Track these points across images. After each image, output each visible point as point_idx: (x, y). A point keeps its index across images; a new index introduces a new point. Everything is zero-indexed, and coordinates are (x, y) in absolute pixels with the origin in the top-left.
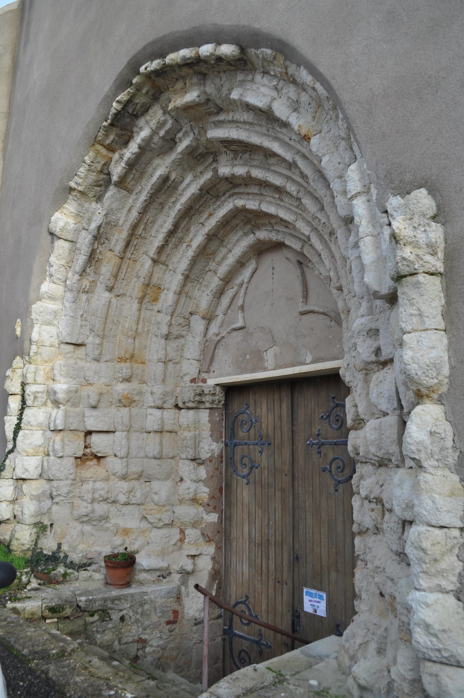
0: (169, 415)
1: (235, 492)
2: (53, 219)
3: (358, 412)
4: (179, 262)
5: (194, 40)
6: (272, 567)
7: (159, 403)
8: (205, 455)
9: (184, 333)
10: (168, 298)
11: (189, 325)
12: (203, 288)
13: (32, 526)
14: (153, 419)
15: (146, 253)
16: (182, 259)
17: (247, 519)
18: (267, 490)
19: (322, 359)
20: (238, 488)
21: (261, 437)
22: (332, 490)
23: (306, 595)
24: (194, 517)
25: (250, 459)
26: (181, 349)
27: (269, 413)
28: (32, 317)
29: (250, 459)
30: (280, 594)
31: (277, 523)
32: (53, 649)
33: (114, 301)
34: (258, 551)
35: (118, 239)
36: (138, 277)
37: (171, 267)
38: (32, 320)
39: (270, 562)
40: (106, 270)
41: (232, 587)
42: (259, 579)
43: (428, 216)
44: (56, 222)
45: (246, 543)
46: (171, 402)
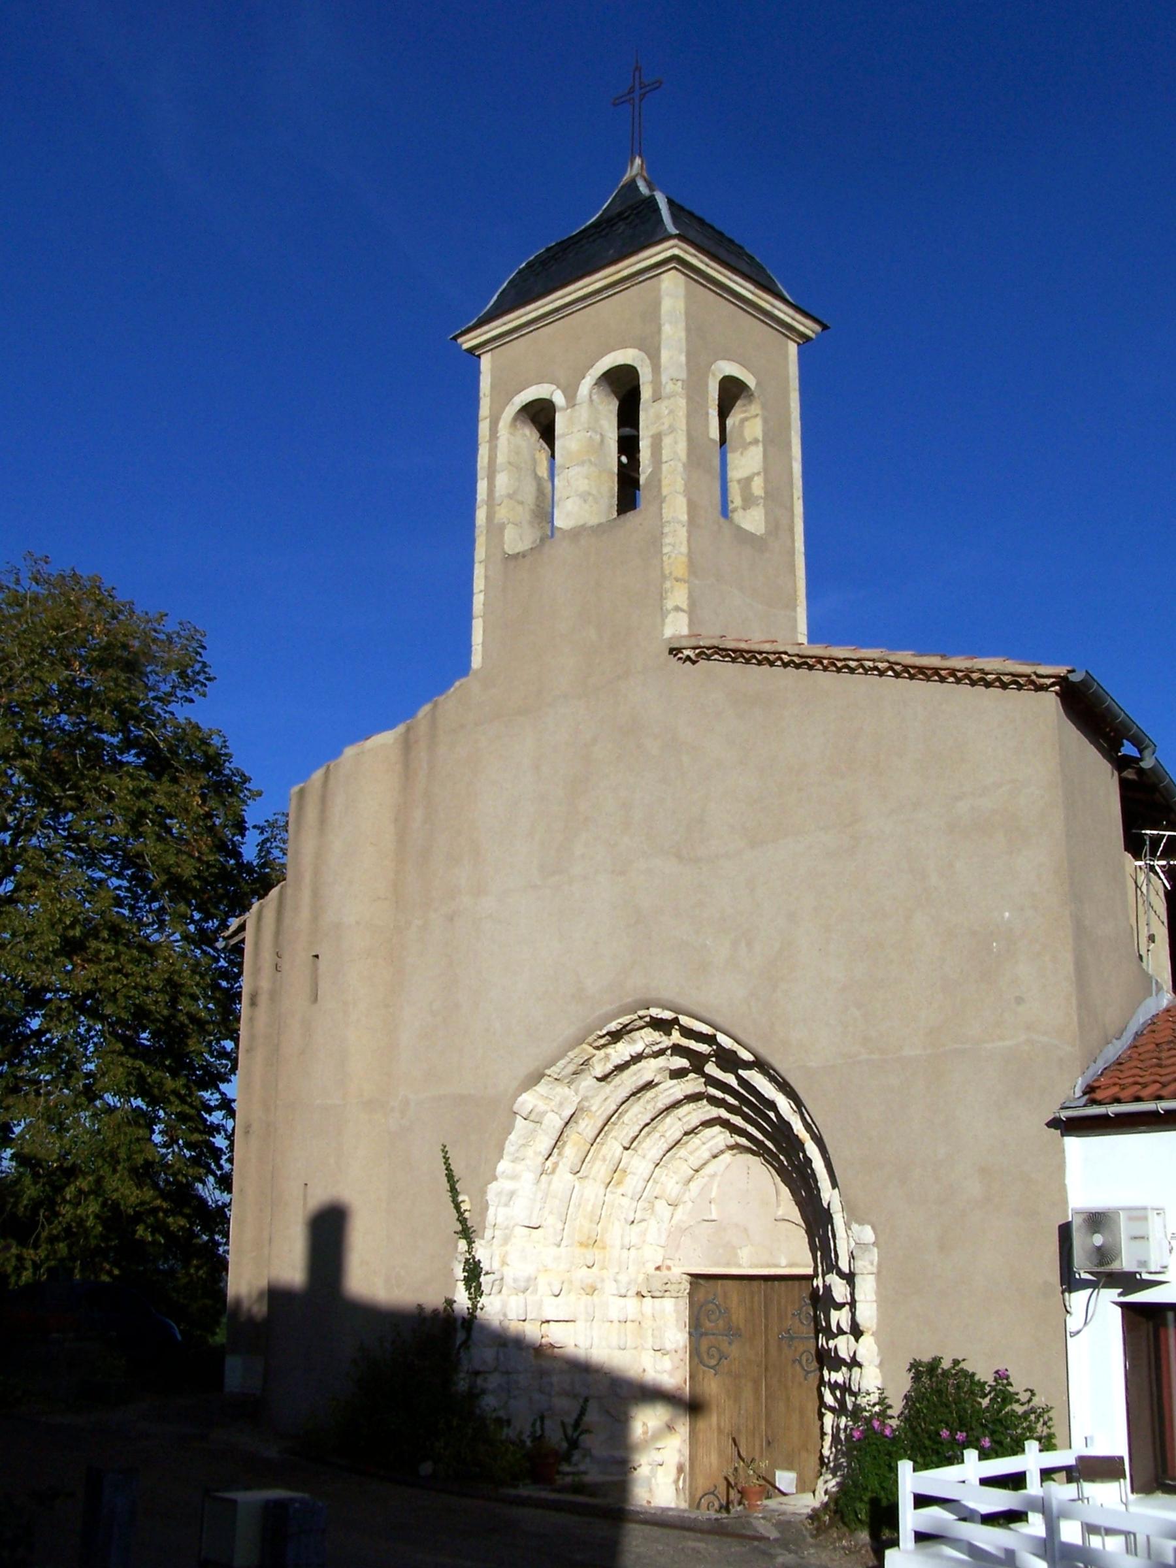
0: (632, 1303)
2: (520, 1099)
4: (649, 1149)
5: (785, 1087)
7: (623, 1292)
8: (669, 1346)
9: (647, 1217)
10: (632, 1183)
11: (653, 1208)
12: (671, 1174)
13: (555, 1437)
14: (617, 1308)
15: (616, 1138)
16: (653, 1146)
21: (730, 1328)
22: (802, 1379)
23: (1121, 1459)
25: (718, 1350)
26: (644, 1233)
29: (718, 1350)
33: (577, 1184)
35: (587, 1127)
36: (604, 1160)
37: (640, 1152)
40: (571, 1152)
44: (523, 1103)
46: (632, 1292)
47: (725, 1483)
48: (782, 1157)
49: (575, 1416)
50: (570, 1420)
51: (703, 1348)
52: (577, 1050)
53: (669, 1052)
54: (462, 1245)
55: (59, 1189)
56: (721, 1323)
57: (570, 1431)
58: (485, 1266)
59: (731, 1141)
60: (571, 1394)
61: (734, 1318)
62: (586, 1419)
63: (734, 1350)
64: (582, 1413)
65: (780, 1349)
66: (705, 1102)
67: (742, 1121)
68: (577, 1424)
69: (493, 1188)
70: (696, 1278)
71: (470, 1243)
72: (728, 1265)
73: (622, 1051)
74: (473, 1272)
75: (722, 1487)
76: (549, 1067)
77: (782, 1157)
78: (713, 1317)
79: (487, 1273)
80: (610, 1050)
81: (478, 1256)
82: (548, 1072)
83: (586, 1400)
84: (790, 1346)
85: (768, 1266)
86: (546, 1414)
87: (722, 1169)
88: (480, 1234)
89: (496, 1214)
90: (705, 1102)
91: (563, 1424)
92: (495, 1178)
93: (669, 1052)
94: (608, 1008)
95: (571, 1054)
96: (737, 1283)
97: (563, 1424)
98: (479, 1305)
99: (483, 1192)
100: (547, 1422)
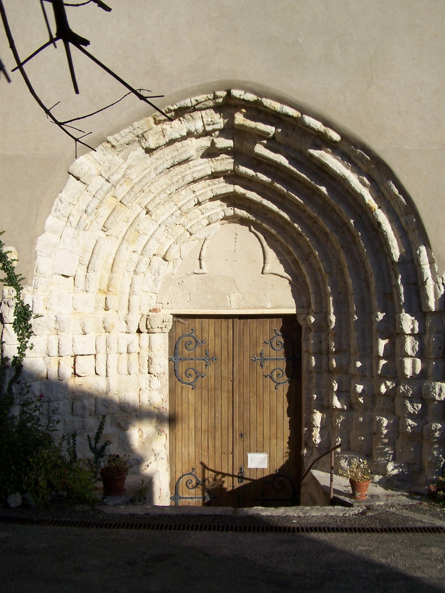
1: (180, 396)
3: (351, 402)
6: (218, 444)
17: (193, 415)
18: (213, 393)
19: (280, 307)
20: (183, 393)
24: (123, 468)
27: (216, 338)
28: (36, 249)
30: (226, 461)
31: (223, 414)
32: (301, 39)
34: (205, 436)
38: (36, 251)
39: (217, 441)
41: (177, 464)
42: (206, 454)
43: (111, 177)
45: (191, 432)
47: (200, 466)
48: (296, 225)
49: (96, 431)
50: (93, 435)
51: (181, 369)
52: (142, 122)
53: (217, 133)
54: (9, 292)
55: (315, 136)
56: (198, 350)
57: (93, 442)
58: (37, 309)
59: (230, 212)
60: (95, 414)
61: (211, 347)
62: (104, 432)
63: (211, 371)
64: (101, 428)
65: (251, 367)
66: (222, 179)
67: (258, 196)
68: (97, 438)
69: (42, 240)
70: (176, 316)
71: (19, 289)
72: (217, 307)
73: (178, 128)
74: (24, 315)
75: (199, 470)
76: (111, 134)
77: (296, 225)
78: (191, 346)
79: (37, 316)
80: (166, 126)
81: (27, 301)
82: (110, 138)
83: (104, 417)
84: (262, 366)
85: (256, 308)
86: (78, 432)
87: (213, 234)
88: (29, 282)
89: (44, 263)
90: (222, 179)
91: (89, 438)
92: (43, 231)
93: (217, 133)
94: (188, 85)
95: (136, 124)
96: (212, 321)
97: (89, 438)
98: (28, 345)
99: (33, 242)
100: (78, 439)
